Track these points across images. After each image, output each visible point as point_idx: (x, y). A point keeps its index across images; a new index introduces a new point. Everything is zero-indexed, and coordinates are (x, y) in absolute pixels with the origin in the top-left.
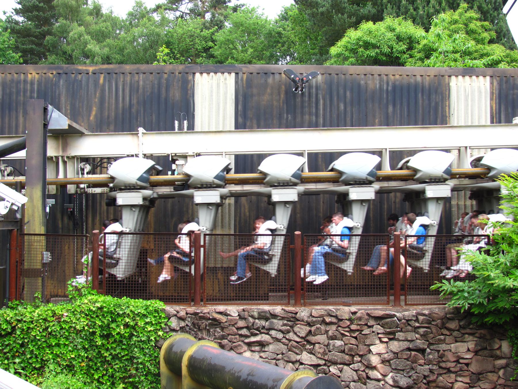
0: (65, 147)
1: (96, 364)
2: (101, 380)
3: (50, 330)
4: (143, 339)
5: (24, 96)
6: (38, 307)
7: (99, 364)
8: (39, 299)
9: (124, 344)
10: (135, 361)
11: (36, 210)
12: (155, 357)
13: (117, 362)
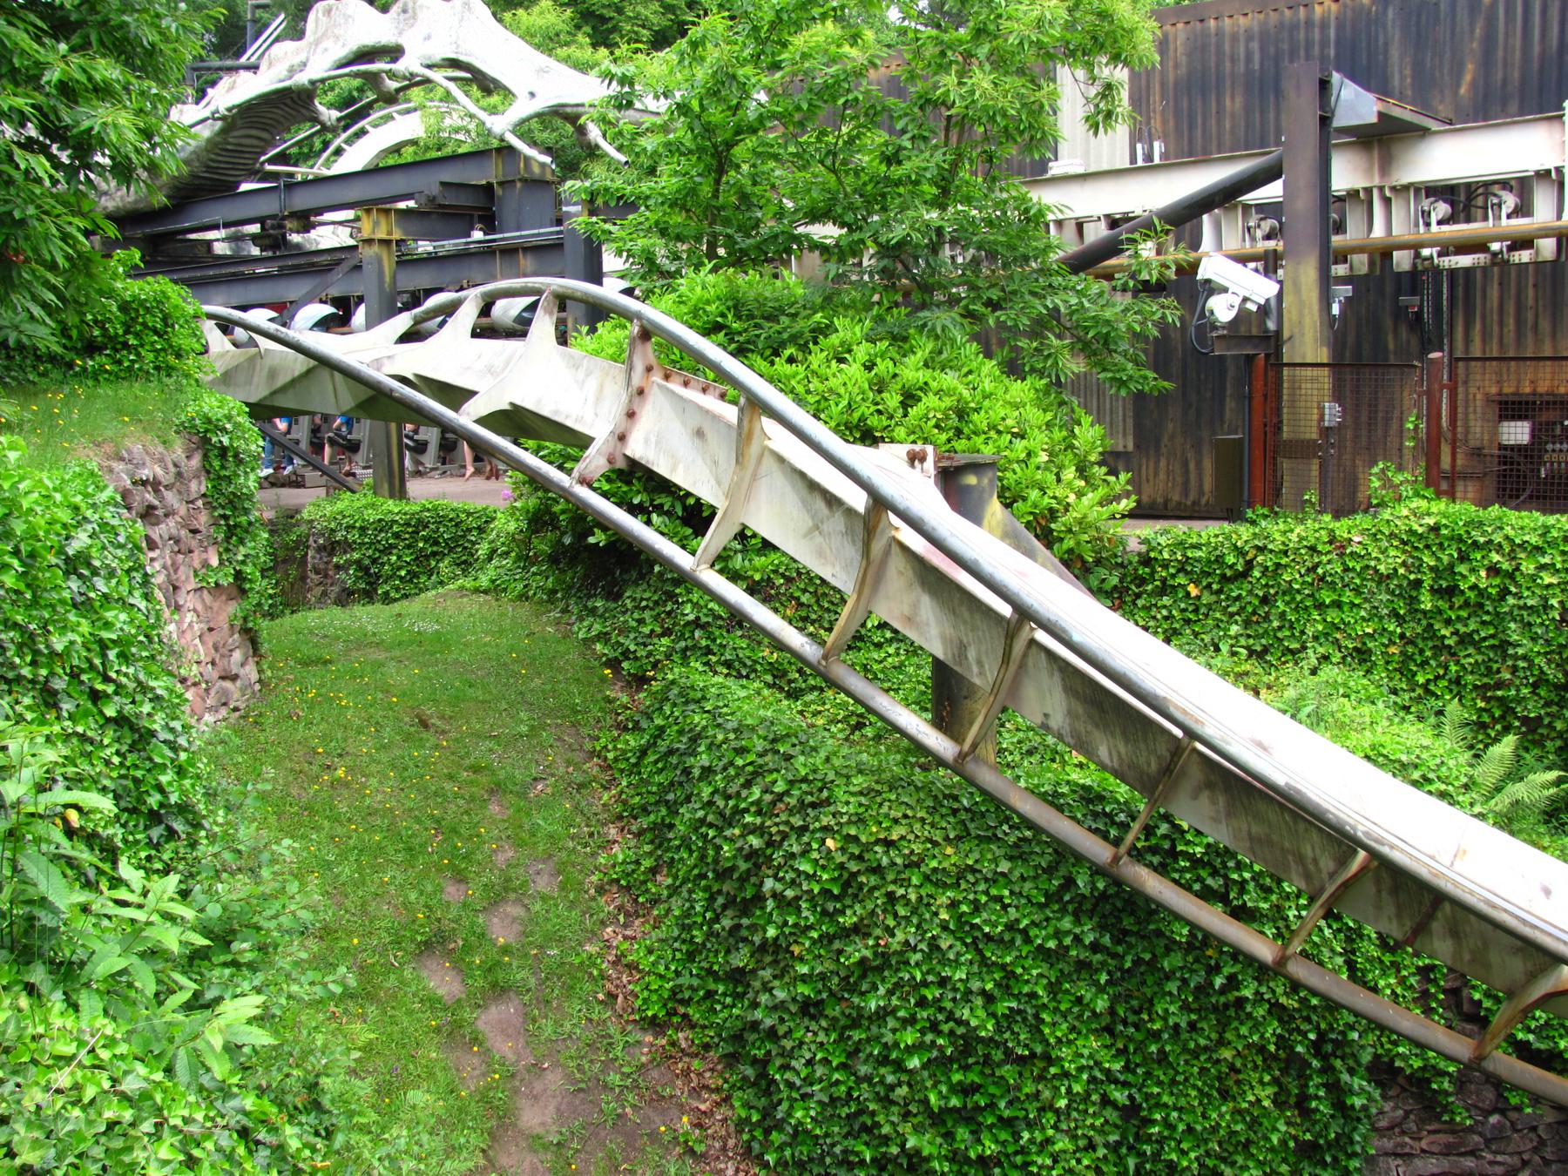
0: (1386, 166)
1: (1421, 652)
2: (1432, 687)
3: (1320, 571)
4: (1530, 602)
7: (1428, 653)
8: (1313, 504)
9: (1488, 613)
10: (1511, 651)
11: (1306, 311)
13: (1471, 650)
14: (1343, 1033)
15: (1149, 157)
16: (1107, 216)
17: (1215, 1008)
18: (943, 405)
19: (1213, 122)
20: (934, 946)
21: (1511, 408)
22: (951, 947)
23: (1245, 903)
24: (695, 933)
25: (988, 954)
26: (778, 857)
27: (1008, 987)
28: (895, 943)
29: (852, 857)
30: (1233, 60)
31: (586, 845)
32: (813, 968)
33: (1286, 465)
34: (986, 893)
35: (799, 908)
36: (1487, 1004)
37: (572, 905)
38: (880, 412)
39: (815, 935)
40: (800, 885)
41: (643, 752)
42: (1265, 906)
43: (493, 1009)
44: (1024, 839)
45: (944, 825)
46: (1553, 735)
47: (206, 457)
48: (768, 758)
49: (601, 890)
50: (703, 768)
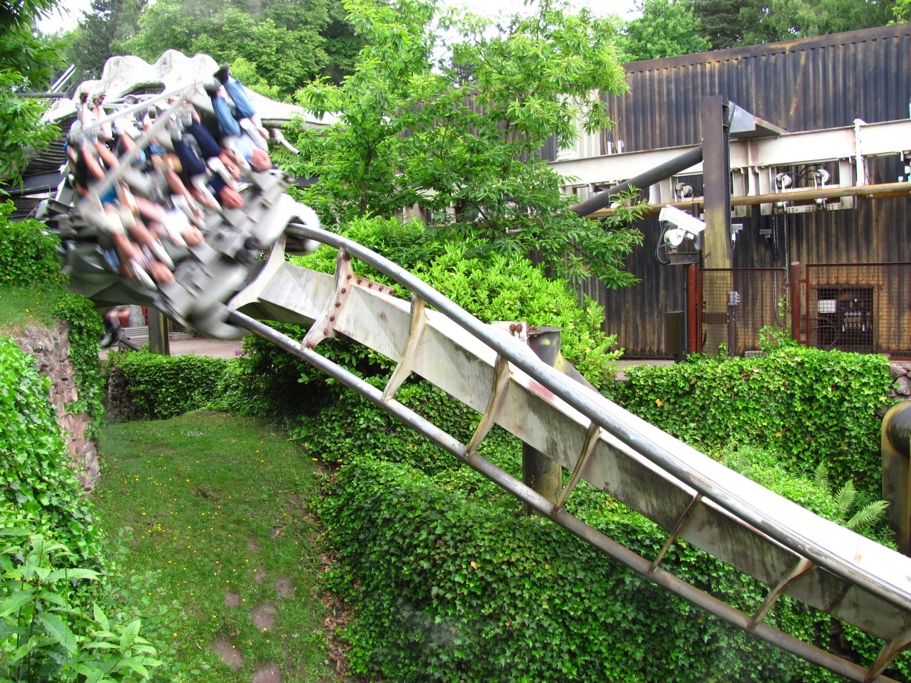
1: (795, 435)
2: (801, 456)
3: (735, 390)
4: (857, 405)
5: (703, 93)
6: (723, 361)
7: (799, 436)
9: (833, 412)
10: (847, 434)
12: (875, 430)
13: (823, 434)
14: (775, 665)
15: (614, 150)
16: (593, 184)
17: (704, 654)
18: (513, 296)
19: (649, 129)
20: (539, 625)
21: (826, 293)
22: (550, 625)
23: (720, 590)
24: (383, 620)
25: (572, 628)
26: (440, 574)
27: (584, 648)
28: (516, 624)
29: (488, 572)
30: (660, 94)
31: (309, 567)
32: (464, 641)
33: (705, 327)
34: (571, 591)
35: (455, 605)
36: (855, 643)
37: (305, 605)
38: (475, 301)
39: (465, 620)
40: (455, 590)
41: (341, 509)
42: (731, 591)
43: (261, 674)
44: (590, 558)
45: (543, 551)
46: (873, 481)
47: (70, 333)
48: (428, 513)
49: (321, 595)
50: (384, 520)
